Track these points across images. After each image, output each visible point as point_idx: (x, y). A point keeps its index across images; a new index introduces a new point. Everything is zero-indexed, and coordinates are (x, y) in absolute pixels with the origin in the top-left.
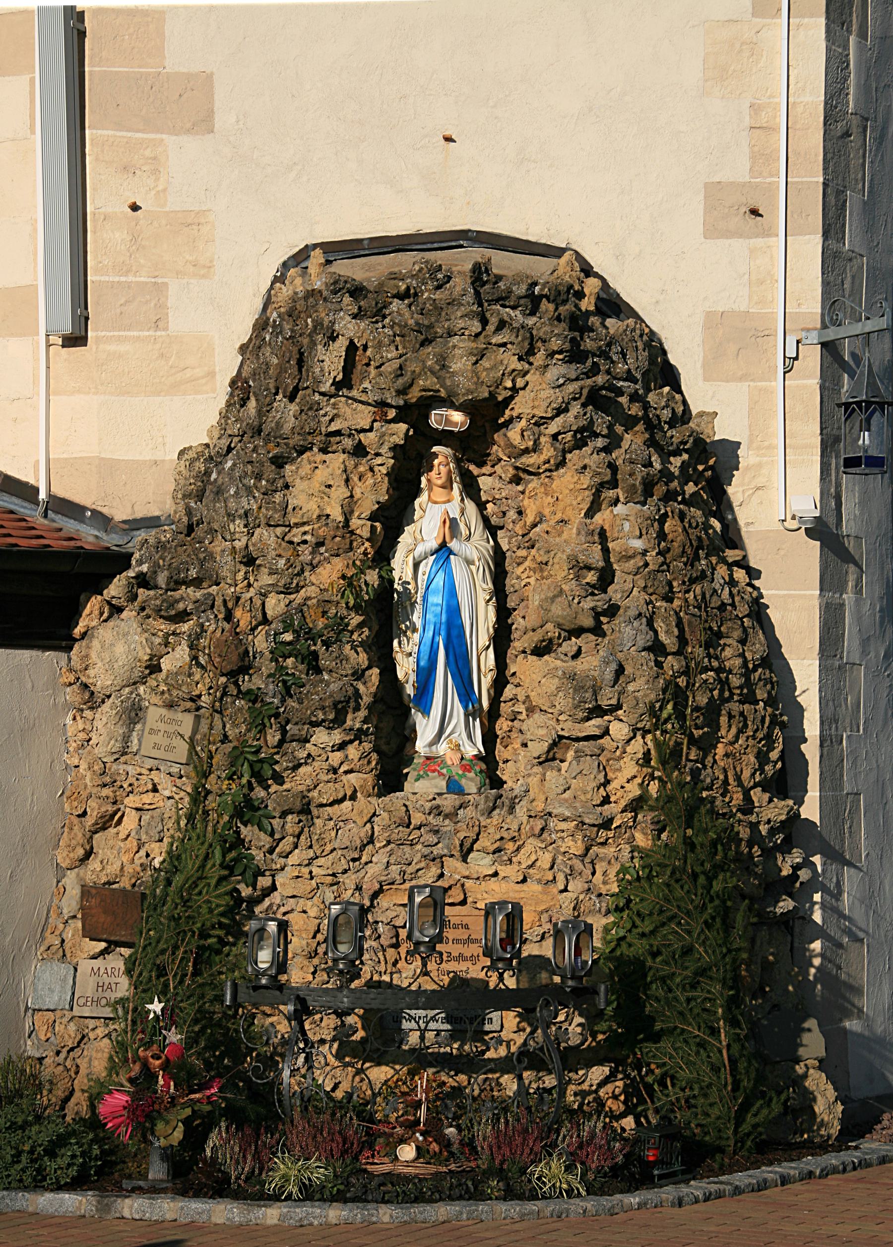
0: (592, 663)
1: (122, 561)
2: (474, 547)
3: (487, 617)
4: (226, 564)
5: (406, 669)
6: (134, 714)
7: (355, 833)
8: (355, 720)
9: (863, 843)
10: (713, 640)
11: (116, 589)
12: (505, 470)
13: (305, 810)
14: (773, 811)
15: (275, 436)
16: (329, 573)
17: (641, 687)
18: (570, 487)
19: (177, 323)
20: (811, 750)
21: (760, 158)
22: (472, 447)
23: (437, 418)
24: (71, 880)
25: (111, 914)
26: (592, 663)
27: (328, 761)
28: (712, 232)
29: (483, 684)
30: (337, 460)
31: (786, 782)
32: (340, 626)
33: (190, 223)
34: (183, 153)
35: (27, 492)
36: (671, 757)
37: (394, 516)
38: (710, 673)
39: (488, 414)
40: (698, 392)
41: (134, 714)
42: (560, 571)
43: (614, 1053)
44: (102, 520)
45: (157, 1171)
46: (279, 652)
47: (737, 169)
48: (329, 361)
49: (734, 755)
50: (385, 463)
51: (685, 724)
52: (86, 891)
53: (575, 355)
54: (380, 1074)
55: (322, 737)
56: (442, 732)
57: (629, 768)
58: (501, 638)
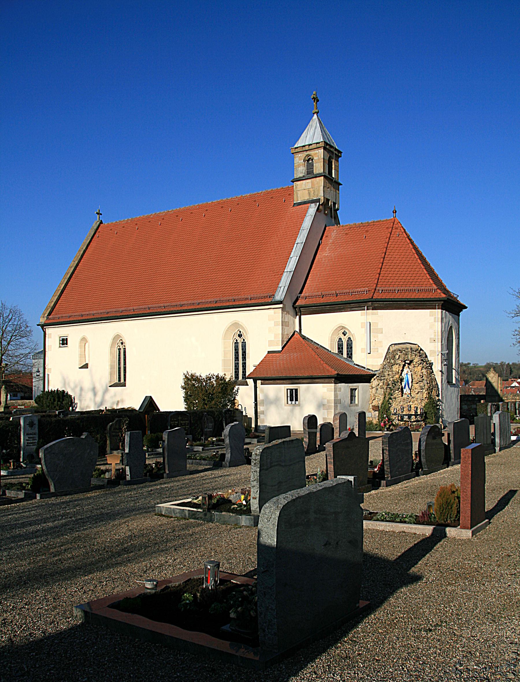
0: (422, 384)
1: (376, 375)
2: (410, 373)
3: (411, 380)
4: (386, 375)
5: (403, 385)
6: (377, 389)
7: (399, 400)
8: (400, 390)
9: (444, 401)
10: (432, 382)
11: (375, 377)
12: (413, 366)
13: (395, 398)
14: (437, 398)
15: (391, 363)
16: (397, 376)
17: (426, 387)
18: (420, 368)
19: (379, 351)
20: (440, 392)
21: (435, 335)
22: (409, 364)
23: (407, 362)
24: (371, 405)
25: (375, 408)
26: (422, 384)
27: (397, 393)
28: (430, 342)
29: (410, 387)
30: (398, 366)
31: (438, 396)
32: (398, 381)
33: (381, 342)
34: (380, 335)
35: (365, 368)
36: (429, 393)
37: (402, 371)
38: (432, 386)
39: (411, 362)
40: (429, 358)
41: (377, 389)
42: (419, 376)
43: (424, 421)
44: (372, 371)
45: (386, 430)
46: (392, 384)
47: (433, 337)
48: (397, 357)
49: (434, 393)
50: (402, 366)
51: (430, 390)
52: (373, 406)
53: (420, 356)
54: (402, 423)
55: (397, 392)
56: (406, 391)
57: (425, 394)
58: (412, 382)
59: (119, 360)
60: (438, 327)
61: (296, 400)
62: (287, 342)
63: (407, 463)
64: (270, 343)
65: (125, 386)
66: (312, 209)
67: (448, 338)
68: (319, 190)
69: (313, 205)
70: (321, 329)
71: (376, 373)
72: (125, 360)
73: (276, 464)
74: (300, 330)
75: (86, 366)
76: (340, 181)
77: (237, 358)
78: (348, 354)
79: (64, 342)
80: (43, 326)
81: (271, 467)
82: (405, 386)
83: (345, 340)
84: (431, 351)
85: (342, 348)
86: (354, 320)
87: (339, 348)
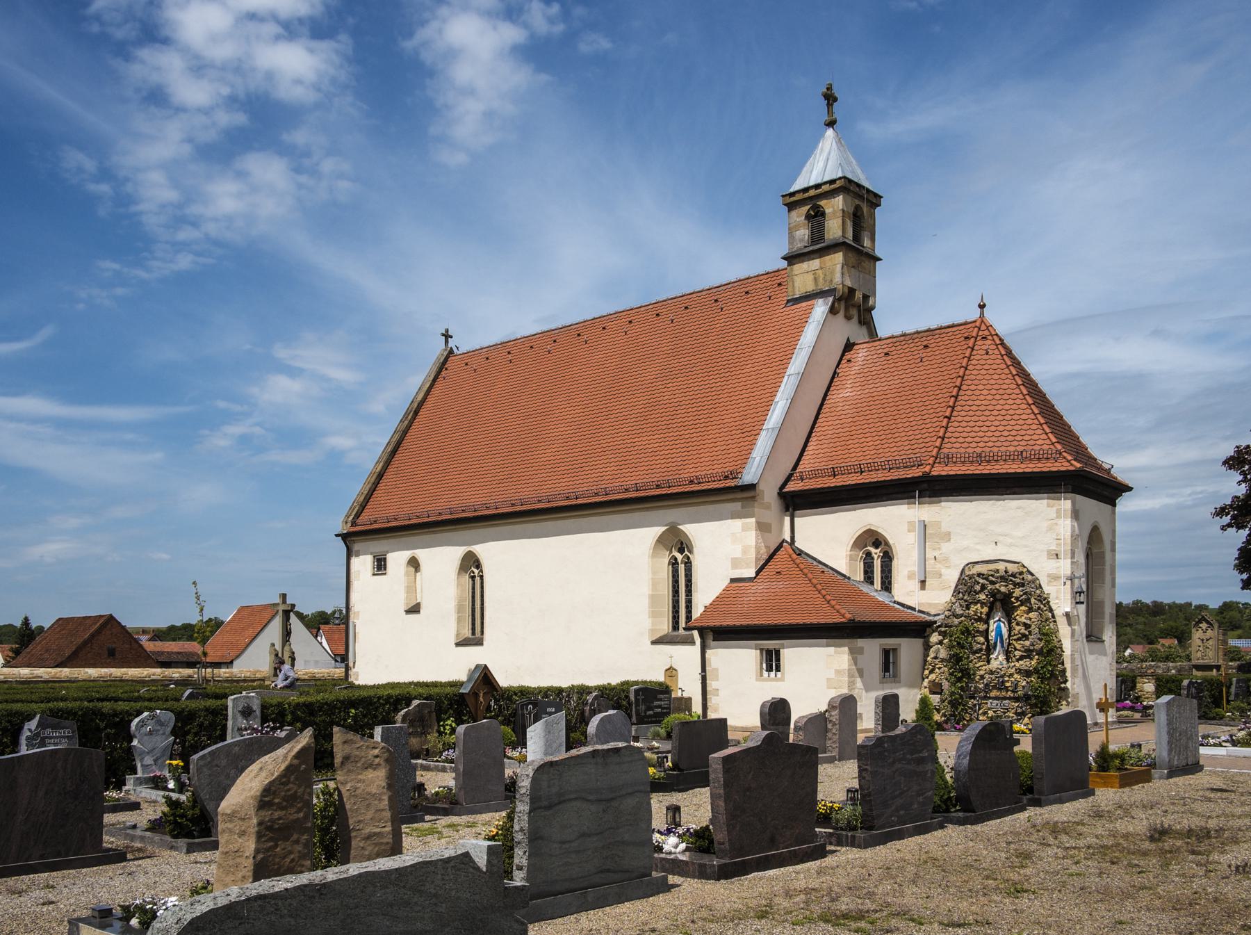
35: (914, 609)
44: (929, 614)
48: (978, 588)
59: (473, 597)
60: (1066, 526)
61: (778, 669)
62: (768, 561)
63: (921, 799)
64: (736, 563)
65: (481, 644)
66: (820, 309)
67: (1095, 551)
68: (833, 272)
69: (821, 301)
70: (828, 537)
71: (936, 618)
72: (482, 596)
73: (572, 796)
74: (793, 538)
75: (414, 609)
76: (878, 253)
77: (676, 592)
78: (883, 583)
79: (381, 565)
80: (345, 537)
81: (560, 803)
82: (995, 644)
83: (876, 553)
84: (1049, 576)
85: (872, 572)
86: (894, 519)
87: (866, 572)
